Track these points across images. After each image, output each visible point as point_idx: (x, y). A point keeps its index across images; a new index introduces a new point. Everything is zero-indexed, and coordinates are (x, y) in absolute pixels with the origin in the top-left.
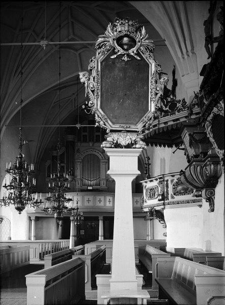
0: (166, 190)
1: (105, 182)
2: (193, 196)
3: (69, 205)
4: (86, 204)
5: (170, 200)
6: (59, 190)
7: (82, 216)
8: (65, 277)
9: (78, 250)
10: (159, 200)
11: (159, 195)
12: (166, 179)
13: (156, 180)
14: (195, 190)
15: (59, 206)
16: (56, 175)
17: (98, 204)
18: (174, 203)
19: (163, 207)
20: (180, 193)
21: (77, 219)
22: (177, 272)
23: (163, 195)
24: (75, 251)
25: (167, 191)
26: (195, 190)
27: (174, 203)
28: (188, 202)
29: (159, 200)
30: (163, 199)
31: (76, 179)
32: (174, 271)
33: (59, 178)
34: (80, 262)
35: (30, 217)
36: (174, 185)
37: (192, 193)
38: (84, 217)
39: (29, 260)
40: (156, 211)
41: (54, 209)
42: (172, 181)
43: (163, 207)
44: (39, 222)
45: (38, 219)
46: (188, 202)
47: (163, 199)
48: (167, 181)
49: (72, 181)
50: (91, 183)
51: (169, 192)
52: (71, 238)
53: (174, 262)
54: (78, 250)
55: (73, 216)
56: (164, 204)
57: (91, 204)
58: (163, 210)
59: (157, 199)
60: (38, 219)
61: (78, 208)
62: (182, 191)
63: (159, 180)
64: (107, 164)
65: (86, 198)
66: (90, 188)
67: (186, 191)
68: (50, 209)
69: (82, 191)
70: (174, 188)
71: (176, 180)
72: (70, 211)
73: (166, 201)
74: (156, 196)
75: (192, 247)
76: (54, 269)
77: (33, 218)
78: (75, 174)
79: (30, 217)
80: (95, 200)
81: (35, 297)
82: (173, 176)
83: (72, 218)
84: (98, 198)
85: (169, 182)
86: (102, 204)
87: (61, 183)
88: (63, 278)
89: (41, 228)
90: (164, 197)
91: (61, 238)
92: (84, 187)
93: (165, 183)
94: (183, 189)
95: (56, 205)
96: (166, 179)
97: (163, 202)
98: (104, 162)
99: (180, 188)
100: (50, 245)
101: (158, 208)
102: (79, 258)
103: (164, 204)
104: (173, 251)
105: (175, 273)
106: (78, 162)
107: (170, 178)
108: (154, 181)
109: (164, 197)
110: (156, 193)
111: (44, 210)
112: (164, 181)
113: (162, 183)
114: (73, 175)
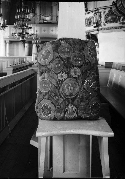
0: (99, 20)
1: (56, 18)
2: (120, 24)
3: (30, 31)
4: (43, 32)
5: (103, 26)
6: (23, 20)
7: (40, 40)
8: (23, 82)
9: (36, 63)
10: (95, 27)
11: (94, 23)
12: (100, 11)
13: (92, 12)
14: (122, 18)
15: (23, 32)
16: (21, 10)
17: (51, 32)
18: (105, 29)
19: (97, 32)
20: (110, 22)
21: (36, 42)
22: (113, 81)
23: (97, 23)
24: (34, 64)
25: (101, 20)
26: (122, 18)
27: (105, 29)
28: (116, 28)
29: (95, 27)
30: (97, 26)
31: (36, 15)
32: (109, 80)
33: (23, 12)
34: (33, 72)
35: (5, 41)
36: (105, 16)
37: (119, 21)
38: (42, 41)
39: (2, 70)
40: (92, 35)
41: (20, 34)
42: (104, 13)
43: (97, 32)
44: (12, 44)
45: (11, 42)
46: (116, 28)
47: (97, 26)
48: (101, 13)
49: (34, 17)
50: (46, 19)
51: (102, 21)
52: (33, 55)
53: (109, 73)
54: (36, 63)
55: (34, 40)
56: (98, 30)
57: (46, 32)
58: (97, 34)
59: (93, 26)
60: (11, 42)
61: (37, 35)
62: (112, 20)
63: (94, 12)
64: (57, 5)
65: (43, 28)
66: (45, 22)
67: (114, 20)
68: (16, 34)
69: (40, 23)
70: (106, 18)
71: (107, 12)
72: (30, 35)
73: (99, 28)
74: (92, 24)
75: (118, 62)
76: (14, 75)
77: (8, 42)
78: (36, 12)
79: (5, 41)
80: (48, 30)
81: (79, 62)
82: (105, 9)
83: (33, 42)
84: (51, 28)
85: (102, 13)
86: (54, 32)
87: (24, 16)
88: (20, 84)
89: (13, 49)
90: (98, 25)
91: (28, 55)
92: (42, 21)
93: (99, 14)
94: (112, 19)
95: (21, 31)
96: (100, 11)
97: (97, 28)
98: (55, 4)
99: (110, 18)
100: (18, 60)
101: (93, 33)
102: (32, 69)
103: (98, 30)
104: (104, 64)
105: (111, 82)
106: (37, 4)
107: (102, 11)
108: (91, 13)
109: (98, 25)
110: (92, 22)
111: (12, 35)
112: (98, 12)
113: (96, 14)
114: (35, 13)
